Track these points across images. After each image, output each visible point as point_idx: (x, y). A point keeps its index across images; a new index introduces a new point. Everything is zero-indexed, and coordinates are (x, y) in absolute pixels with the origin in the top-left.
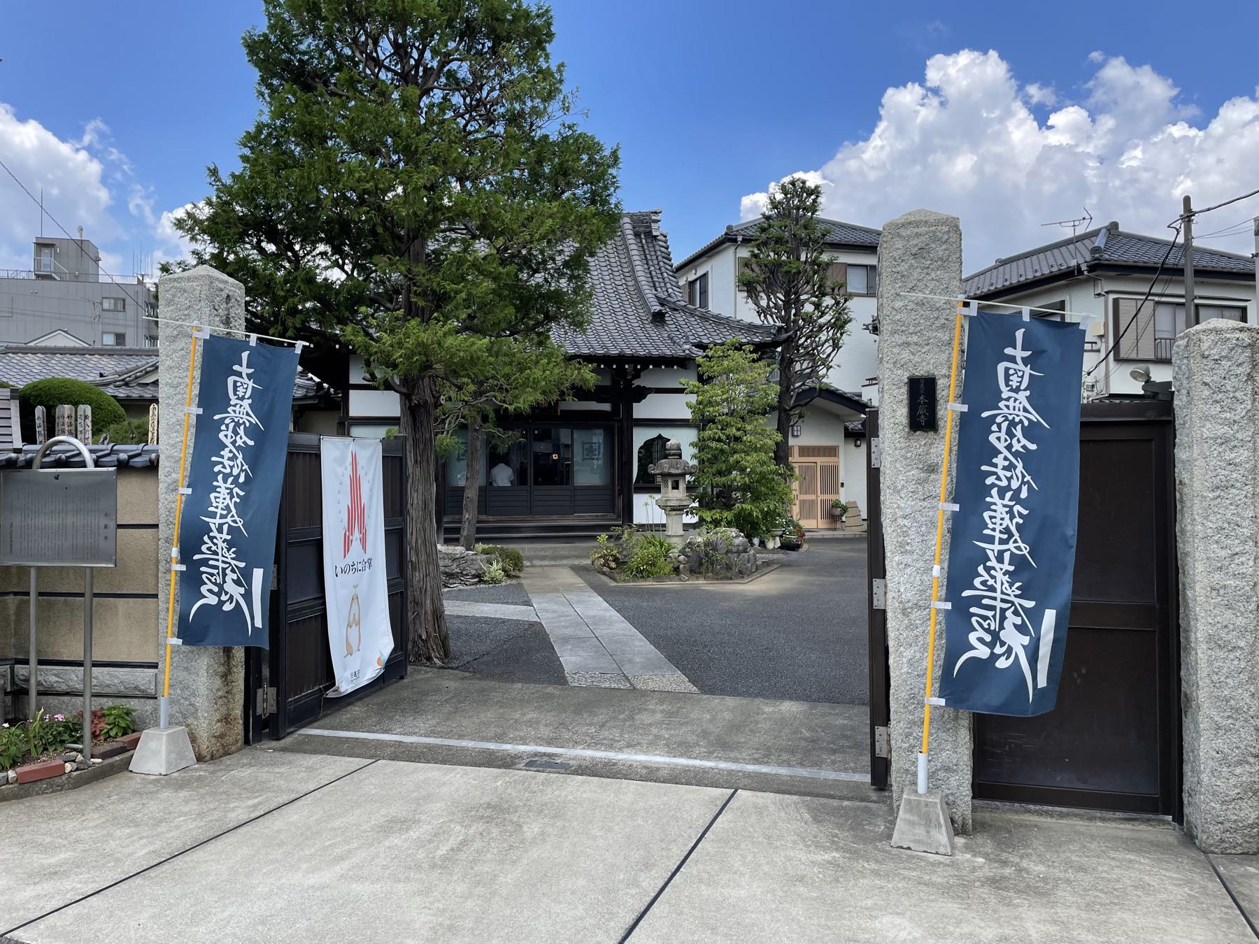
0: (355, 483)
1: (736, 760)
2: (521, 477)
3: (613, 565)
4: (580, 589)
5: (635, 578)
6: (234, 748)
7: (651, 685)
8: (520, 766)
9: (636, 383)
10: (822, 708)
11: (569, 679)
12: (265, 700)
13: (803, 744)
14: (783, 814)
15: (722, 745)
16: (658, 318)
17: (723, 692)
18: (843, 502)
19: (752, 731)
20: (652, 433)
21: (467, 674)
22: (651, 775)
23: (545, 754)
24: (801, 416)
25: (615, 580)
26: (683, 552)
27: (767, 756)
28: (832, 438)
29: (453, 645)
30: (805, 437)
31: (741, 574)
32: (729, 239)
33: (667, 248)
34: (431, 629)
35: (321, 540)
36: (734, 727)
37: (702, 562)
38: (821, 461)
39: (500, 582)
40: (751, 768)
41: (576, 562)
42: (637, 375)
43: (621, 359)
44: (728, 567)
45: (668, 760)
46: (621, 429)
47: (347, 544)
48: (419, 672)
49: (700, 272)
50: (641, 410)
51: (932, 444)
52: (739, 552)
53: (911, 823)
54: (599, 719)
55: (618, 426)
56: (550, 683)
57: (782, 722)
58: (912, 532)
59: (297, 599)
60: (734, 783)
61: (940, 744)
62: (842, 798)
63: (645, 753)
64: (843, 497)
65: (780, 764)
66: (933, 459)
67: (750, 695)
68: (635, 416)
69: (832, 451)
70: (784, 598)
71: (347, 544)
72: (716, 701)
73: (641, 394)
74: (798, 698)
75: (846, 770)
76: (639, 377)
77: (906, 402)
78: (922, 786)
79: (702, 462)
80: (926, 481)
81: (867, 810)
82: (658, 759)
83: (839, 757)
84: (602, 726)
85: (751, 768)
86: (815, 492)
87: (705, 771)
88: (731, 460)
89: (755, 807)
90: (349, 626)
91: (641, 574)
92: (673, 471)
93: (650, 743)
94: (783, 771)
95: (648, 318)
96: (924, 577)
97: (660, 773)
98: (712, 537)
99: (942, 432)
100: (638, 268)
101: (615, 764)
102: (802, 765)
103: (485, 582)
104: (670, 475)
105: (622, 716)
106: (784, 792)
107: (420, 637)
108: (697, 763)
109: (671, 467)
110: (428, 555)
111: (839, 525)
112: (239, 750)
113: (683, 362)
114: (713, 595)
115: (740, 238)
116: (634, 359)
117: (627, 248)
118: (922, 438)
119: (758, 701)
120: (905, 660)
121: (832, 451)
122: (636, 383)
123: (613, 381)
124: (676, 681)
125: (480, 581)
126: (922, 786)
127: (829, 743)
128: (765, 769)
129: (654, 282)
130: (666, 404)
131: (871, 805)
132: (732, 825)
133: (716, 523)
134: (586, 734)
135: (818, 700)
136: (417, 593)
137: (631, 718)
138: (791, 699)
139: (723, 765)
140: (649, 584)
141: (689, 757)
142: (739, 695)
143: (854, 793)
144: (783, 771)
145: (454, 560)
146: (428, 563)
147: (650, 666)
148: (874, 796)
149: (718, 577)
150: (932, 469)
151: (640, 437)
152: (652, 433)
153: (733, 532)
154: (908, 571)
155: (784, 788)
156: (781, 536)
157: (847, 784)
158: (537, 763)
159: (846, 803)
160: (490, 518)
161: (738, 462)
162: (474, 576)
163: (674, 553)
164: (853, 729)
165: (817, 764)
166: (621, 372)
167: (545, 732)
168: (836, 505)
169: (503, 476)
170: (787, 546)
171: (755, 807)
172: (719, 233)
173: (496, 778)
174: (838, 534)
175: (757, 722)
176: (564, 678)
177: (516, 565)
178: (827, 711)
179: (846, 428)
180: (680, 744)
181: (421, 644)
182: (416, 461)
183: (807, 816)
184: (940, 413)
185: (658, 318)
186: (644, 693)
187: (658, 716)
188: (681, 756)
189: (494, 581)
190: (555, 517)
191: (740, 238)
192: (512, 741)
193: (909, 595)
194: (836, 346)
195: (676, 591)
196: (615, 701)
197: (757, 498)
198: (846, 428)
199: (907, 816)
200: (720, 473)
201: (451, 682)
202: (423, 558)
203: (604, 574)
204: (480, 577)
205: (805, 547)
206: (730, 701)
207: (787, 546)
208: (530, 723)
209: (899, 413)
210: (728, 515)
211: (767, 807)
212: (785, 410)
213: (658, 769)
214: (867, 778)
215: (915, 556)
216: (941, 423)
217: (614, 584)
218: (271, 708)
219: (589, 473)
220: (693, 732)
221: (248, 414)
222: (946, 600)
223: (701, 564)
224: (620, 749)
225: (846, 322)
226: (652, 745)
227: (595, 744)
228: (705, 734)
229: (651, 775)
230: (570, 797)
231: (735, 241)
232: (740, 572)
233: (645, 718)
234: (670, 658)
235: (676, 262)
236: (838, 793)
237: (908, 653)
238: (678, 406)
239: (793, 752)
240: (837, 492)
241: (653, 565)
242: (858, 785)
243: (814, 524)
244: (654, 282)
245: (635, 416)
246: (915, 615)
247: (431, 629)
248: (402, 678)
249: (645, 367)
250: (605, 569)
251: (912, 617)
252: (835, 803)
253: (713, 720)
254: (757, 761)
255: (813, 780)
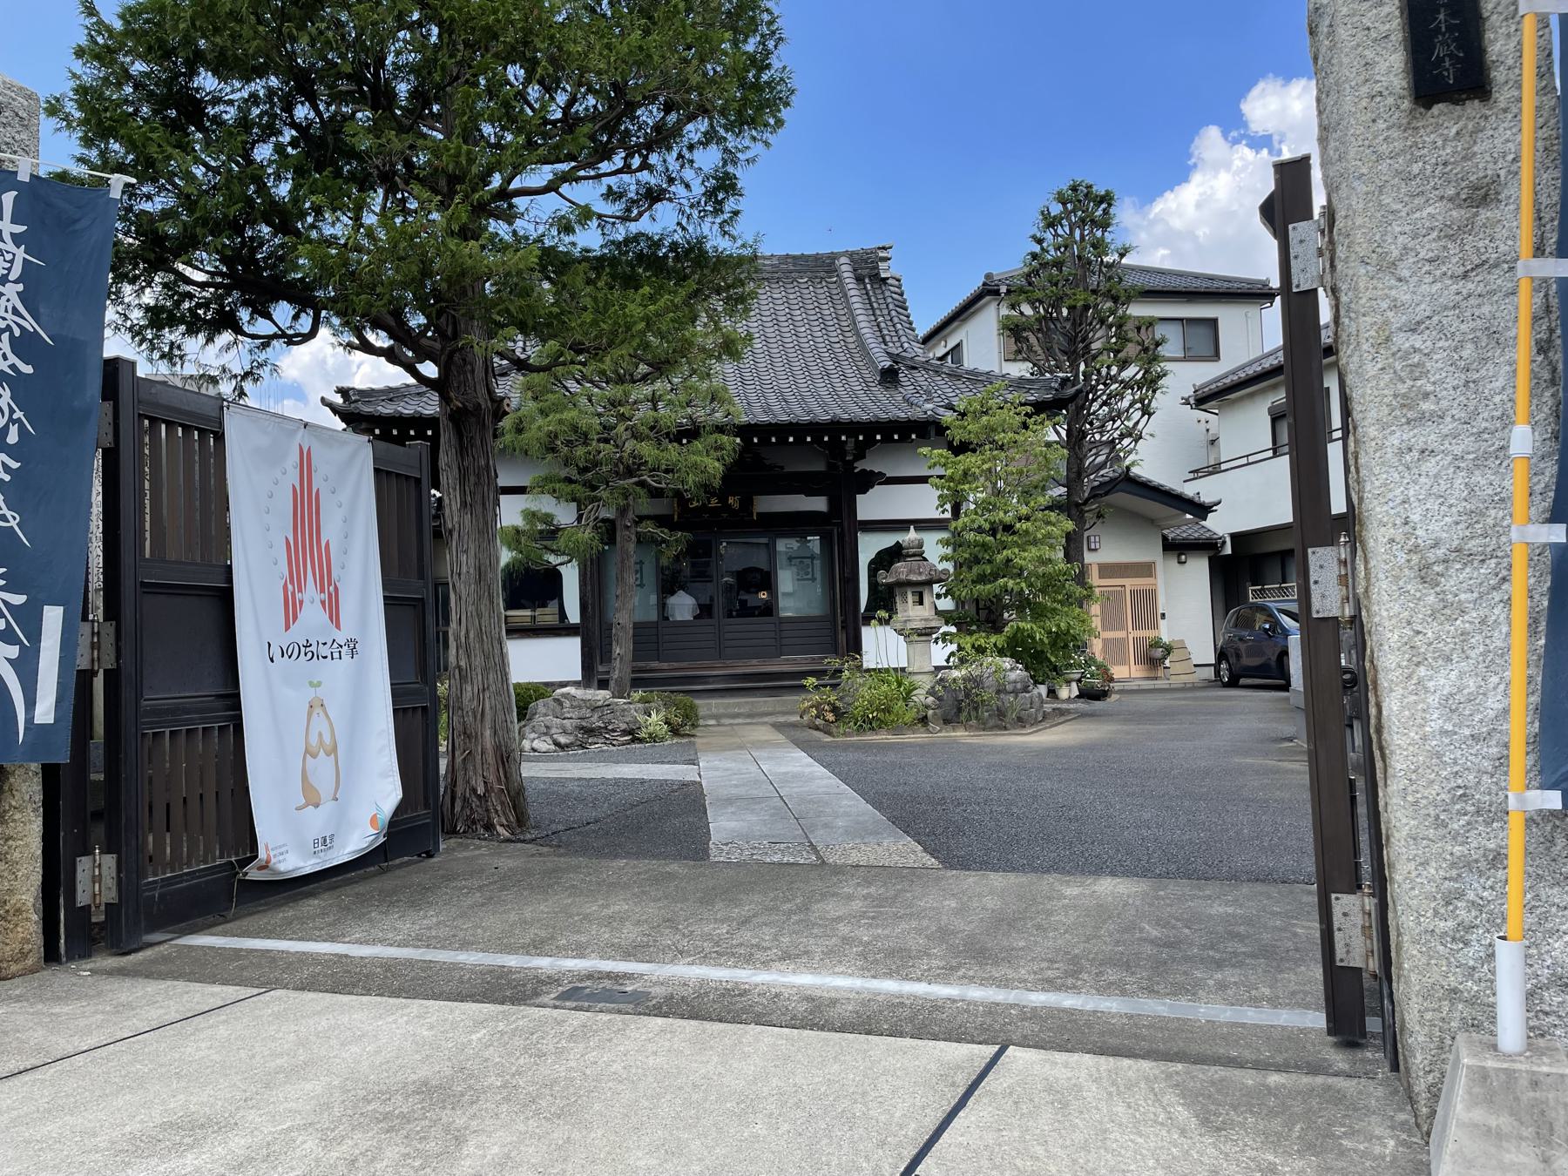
0: (306, 508)
1: (1004, 983)
2: (705, 611)
3: (830, 717)
4: (778, 745)
5: (860, 730)
6: (14, 968)
7: (854, 858)
8: (545, 999)
9: (860, 466)
10: (1174, 888)
11: (713, 851)
12: (96, 879)
13: (1148, 949)
14: (1120, 1109)
15: (976, 954)
16: (889, 377)
17: (985, 865)
18: (1166, 639)
19: (1039, 927)
20: (887, 540)
21: (546, 849)
22: (816, 1016)
23: (609, 975)
24: (1100, 516)
25: (829, 733)
26: (932, 692)
27: (1075, 974)
28: (1146, 551)
29: (532, 812)
30: (1108, 549)
31: (1021, 722)
32: (989, 291)
33: (899, 287)
34: (492, 778)
35: (231, 589)
36: (1003, 922)
37: (961, 705)
38: (1130, 583)
39: (662, 739)
40: (1038, 998)
41: (782, 719)
42: (861, 456)
43: (835, 427)
44: (1001, 713)
45: (857, 983)
46: (841, 536)
47: (291, 611)
48: (467, 847)
49: (951, 343)
50: (870, 506)
51: (1478, 130)
52: (1015, 692)
53: (1495, 1136)
54: (746, 910)
55: (839, 529)
56: (679, 856)
57: (1102, 911)
58: (1437, 365)
59: (1028, 1027)
60: (998, 1032)
61: (1545, 917)
62: (1261, 1066)
63: (815, 970)
64: (1165, 633)
65: (1104, 989)
66: (1482, 167)
67: (1035, 870)
68: (859, 518)
69: (1146, 570)
70: (1091, 747)
71: (291, 611)
72: (970, 879)
73: (868, 481)
74: (1128, 873)
75: (1255, 1002)
76: (864, 457)
77: (1397, 37)
78: (1511, 1028)
79: (959, 566)
80: (1467, 227)
81: (1338, 1098)
82: (842, 983)
83: (1230, 975)
84: (745, 922)
85: (1038, 998)
86: (1122, 627)
87: (936, 1006)
88: (999, 558)
89: (1049, 1089)
90: (309, 752)
91: (869, 724)
92: (914, 578)
93: (829, 953)
94: (1111, 1005)
95: (873, 377)
96: (1477, 477)
97: (833, 1013)
98: (974, 670)
99: (1502, 96)
100: (860, 318)
101: (744, 993)
102: (1151, 991)
103: (641, 741)
104: (910, 584)
105: (787, 906)
106: (1116, 1052)
107: (474, 790)
108: (921, 988)
109: (910, 571)
110: (487, 657)
111: (1160, 673)
112: (33, 971)
113: (929, 430)
114: (973, 750)
115: (1003, 289)
116: (853, 427)
117: (845, 295)
118: (1448, 121)
119: (1050, 878)
120: (1433, 700)
121: (1146, 570)
122: (860, 466)
123: (829, 465)
124: (904, 851)
125: (635, 740)
126: (1511, 1028)
127: (1203, 947)
128: (1068, 1001)
129: (883, 337)
130: (903, 501)
131: (1341, 1083)
132: (990, 1138)
133: (981, 650)
134: (707, 937)
135: (1167, 875)
136: (469, 719)
137: (804, 908)
138: (1113, 874)
139: (976, 993)
140: (882, 737)
141: (907, 978)
142: (1014, 870)
143: (1285, 1054)
144: (1111, 1005)
145: (594, 709)
146: (486, 670)
147: (860, 831)
148: (1340, 1059)
149: (984, 726)
150: (1483, 195)
151: (869, 547)
152: (887, 540)
153: (1007, 663)
154: (1430, 465)
155: (1113, 1041)
156: (1079, 681)
157: (1265, 1032)
158: (578, 994)
159: (1274, 1079)
160: (665, 665)
161: (1009, 560)
162: (625, 733)
163: (920, 697)
164: (1249, 921)
165: (1188, 989)
166: (836, 448)
167: (630, 934)
168: (1157, 643)
169: (683, 606)
170: (1089, 694)
171: (1049, 1089)
172: (975, 284)
173: (479, 1024)
174: (1160, 684)
175: (1049, 913)
176: (706, 852)
177: (687, 716)
178: (1187, 890)
179: (1165, 538)
180: (890, 953)
181: (475, 802)
182: (464, 504)
183: (1182, 1113)
184: (1497, 45)
185: (889, 377)
186: (838, 870)
187: (857, 905)
188: (889, 975)
189: (653, 738)
190: (754, 662)
191: (1003, 289)
192: (562, 951)
193: (1438, 527)
194: (1147, 412)
195: (921, 746)
196: (790, 883)
197: (1039, 613)
198: (1165, 538)
199: (1478, 1115)
200: (982, 579)
201: (510, 860)
202: (478, 661)
203: (817, 728)
204: (633, 735)
205: (1114, 697)
206: (997, 879)
207: (1089, 694)
208: (609, 921)
209: (1382, 67)
210: (998, 640)
211: (1078, 1088)
212: (1077, 505)
213: (834, 1002)
214: (1317, 1020)
215: (1448, 426)
216: (1498, 75)
217: (830, 739)
218: (109, 893)
219: (796, 593)
220: (919, 931)
221: (15, 312)
222: (1554, 519)
223: (960, 710)
224: (766, 964)
225: (1160, 377)
226: (832, 958)
227: (720, 953)
228: (944, 934)
229: (816, 1016)
230: (616, 1067)
231: (997, 293)
232: (1020, 719)
233: (832, 908)
234: (895, 820)
235: (922, 330)
236: (1248, 1054)
237: (1444, 681)
238: (924, 502)
239: (1127, 966)
240: (1156, 627)
241: (888, 710)
242: (1292, 1037)
243: (1127, 672)
244: (883, 337)
245: (859, 518)
246: (1457, 580)
247: (492, 778)
248: (430, 855)
249: (870, 442)
250: (819, 722)
251: (1449, 584)
252: (1249, 1078)
253: (959, 912)
254: (1050, 985)
255: (1184, 1026)
